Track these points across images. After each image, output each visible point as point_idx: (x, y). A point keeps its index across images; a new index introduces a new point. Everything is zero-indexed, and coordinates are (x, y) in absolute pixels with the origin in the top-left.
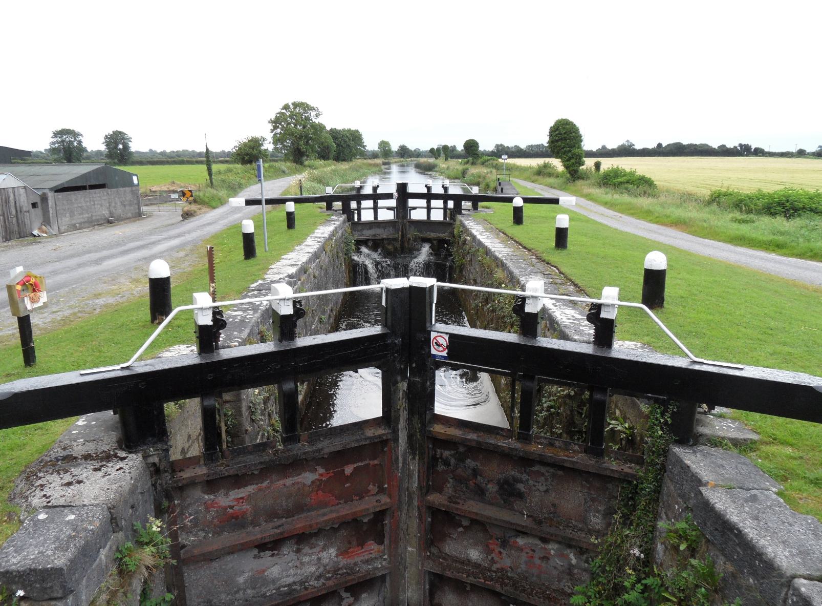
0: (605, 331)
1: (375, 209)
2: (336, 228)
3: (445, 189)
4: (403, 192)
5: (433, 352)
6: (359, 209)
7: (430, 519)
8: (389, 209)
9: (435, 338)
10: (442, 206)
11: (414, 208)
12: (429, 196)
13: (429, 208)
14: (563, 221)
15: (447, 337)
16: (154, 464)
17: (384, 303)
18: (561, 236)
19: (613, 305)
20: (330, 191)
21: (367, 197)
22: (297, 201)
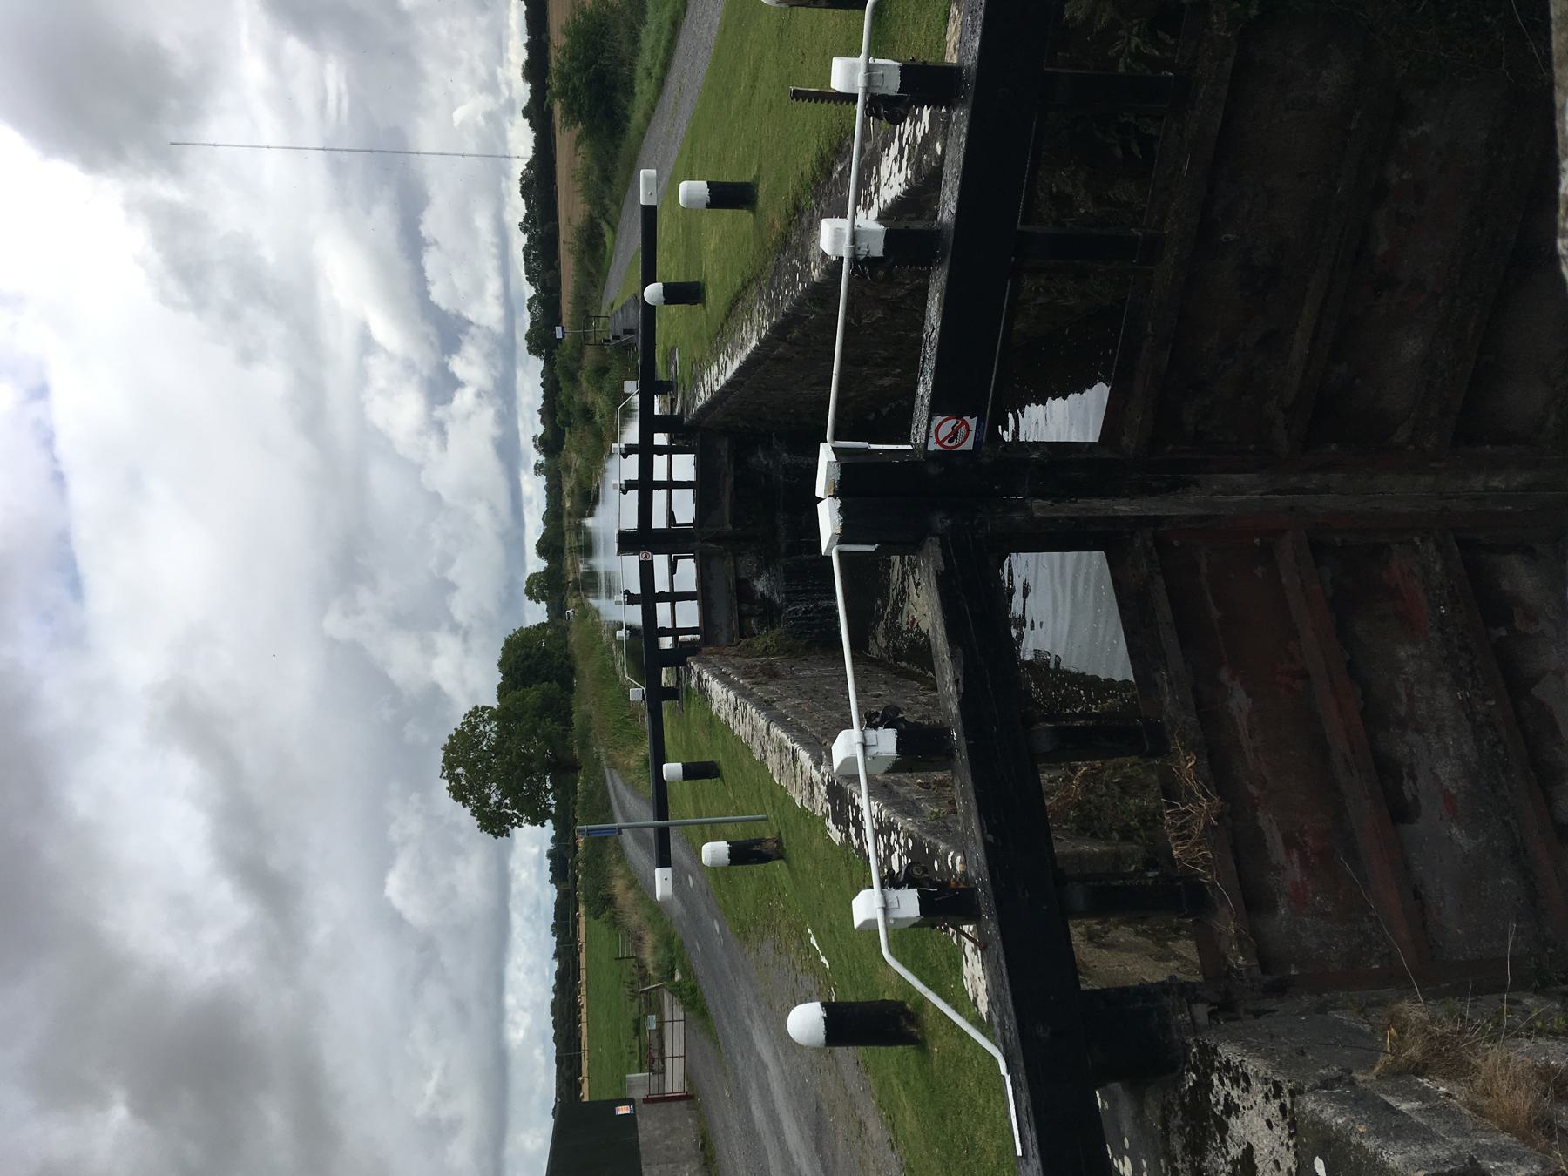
0: (925, 84)
1: (673, 597)
2: (715, 676)
3: (629, 450)
4: (638, 540)
5: (968, 446)
6: (674, 632)
7: (1333, 447)
8: (673, 568)
9: (938, 442)
10: (664, 492)
11: (671, 516)
12: (645, 485)
13: (670, 485)
14: (692, 190)
15: (939, 419)
16: (1211, 1014)
17: (871, 548)
18: (726, 196)
19: (870, 69)
20: (636, 693)
21: (649, 615)
22: (659, 757)
